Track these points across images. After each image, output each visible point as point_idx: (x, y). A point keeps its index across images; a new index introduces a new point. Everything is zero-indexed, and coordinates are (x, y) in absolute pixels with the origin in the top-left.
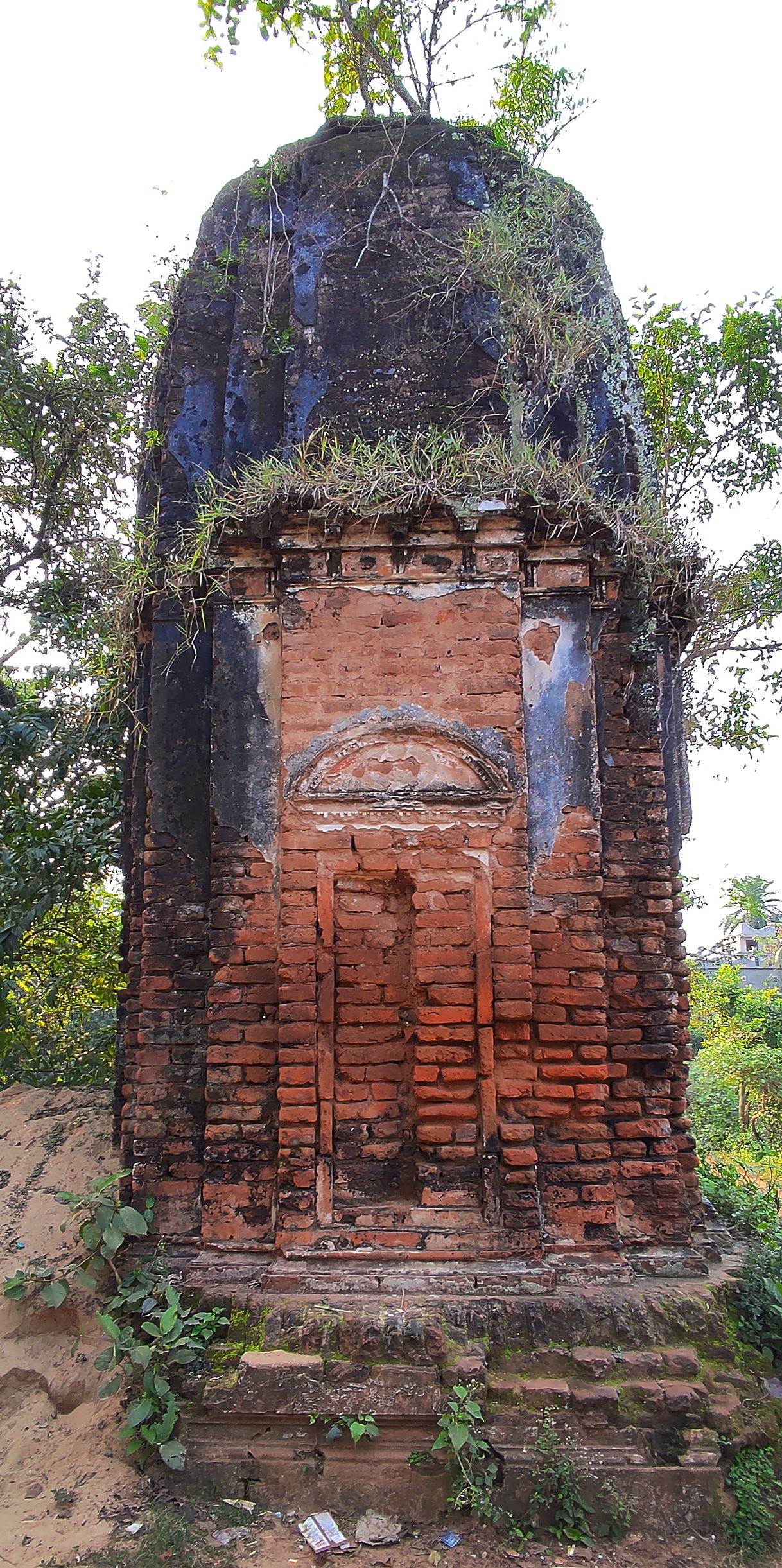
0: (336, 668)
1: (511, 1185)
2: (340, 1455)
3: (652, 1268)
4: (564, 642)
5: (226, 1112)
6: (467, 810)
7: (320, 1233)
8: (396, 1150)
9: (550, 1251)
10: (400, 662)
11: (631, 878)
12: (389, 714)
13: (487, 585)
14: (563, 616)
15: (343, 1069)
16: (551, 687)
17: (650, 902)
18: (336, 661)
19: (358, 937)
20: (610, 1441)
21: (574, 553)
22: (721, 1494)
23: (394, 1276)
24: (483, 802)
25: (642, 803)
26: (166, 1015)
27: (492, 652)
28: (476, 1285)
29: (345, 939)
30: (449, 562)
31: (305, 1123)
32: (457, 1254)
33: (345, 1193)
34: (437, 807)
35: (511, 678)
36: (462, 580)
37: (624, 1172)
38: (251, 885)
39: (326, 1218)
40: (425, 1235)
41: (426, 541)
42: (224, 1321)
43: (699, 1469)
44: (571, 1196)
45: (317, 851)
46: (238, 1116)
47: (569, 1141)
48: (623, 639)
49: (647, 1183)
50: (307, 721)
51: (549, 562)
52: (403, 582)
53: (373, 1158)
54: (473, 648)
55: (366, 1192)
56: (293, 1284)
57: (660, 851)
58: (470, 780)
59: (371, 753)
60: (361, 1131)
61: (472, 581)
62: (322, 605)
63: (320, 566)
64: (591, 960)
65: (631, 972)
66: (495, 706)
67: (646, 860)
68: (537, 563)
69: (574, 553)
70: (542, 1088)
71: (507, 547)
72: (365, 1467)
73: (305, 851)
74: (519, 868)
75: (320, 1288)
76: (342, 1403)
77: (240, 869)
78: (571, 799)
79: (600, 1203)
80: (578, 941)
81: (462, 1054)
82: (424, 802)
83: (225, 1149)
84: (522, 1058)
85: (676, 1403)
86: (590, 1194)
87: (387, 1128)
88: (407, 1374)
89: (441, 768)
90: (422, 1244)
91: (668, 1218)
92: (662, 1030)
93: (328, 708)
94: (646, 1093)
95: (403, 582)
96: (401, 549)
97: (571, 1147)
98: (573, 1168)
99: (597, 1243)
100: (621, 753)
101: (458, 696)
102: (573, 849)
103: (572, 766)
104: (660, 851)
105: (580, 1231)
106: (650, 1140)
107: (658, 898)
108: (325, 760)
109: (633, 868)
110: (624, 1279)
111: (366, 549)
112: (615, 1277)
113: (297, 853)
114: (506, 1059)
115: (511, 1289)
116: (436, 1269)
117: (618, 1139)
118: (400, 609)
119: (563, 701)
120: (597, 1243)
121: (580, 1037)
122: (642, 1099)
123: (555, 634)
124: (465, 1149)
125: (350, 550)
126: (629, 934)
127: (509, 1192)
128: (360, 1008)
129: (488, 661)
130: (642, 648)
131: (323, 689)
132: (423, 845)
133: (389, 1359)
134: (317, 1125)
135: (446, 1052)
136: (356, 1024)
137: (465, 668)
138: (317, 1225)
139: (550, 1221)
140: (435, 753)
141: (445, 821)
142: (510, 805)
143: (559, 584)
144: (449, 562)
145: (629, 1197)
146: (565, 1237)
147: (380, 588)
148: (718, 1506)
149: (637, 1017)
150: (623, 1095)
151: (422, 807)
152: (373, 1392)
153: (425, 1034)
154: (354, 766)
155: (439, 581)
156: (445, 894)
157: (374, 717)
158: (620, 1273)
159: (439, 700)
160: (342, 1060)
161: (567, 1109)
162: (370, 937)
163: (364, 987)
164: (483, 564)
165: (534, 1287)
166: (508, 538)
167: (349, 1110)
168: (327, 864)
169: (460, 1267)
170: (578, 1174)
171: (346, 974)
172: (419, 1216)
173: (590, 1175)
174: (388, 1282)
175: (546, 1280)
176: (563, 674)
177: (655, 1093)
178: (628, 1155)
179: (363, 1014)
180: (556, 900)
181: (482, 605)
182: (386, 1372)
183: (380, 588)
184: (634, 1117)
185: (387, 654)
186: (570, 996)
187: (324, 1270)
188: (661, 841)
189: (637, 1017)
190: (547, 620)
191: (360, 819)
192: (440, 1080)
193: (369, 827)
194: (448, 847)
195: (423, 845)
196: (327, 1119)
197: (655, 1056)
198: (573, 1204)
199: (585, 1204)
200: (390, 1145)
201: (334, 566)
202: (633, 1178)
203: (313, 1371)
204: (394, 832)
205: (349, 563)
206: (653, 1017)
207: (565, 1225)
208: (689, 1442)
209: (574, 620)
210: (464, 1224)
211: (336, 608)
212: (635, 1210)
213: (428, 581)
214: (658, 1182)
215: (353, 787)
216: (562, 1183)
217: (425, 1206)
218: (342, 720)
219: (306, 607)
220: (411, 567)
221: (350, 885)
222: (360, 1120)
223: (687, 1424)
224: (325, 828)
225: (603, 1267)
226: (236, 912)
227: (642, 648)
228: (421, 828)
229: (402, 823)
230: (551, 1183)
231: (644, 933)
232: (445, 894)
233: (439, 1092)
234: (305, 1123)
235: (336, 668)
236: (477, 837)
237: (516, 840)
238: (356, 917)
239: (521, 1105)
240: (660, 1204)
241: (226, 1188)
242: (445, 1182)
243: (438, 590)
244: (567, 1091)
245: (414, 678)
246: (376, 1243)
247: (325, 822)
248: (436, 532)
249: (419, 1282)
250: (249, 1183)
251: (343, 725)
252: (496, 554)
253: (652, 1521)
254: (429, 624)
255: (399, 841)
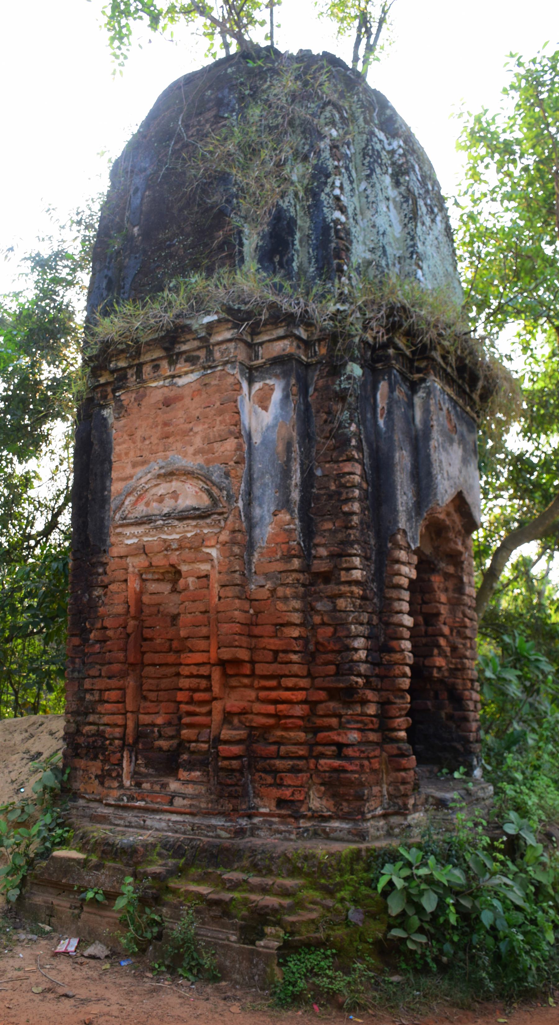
0: (138, 439)
1: (222, 769)
2: (90, 910)
3: (327, 834)
4: (277, 395)
5: (91, 718)
6: (201, 522)
7: (122, 792)
8: (175, 745)
9: (256, 815)
10: (171, 429)
11: (332, 556)
12: (163, 464)
13: (219, 368)
14: (277, 376)
15: (144, 693)
16: (268, 428)
17: (343, 573)
18: (139, 434)
19: (154, 609)
20: (224, 926)
21: (281, 332)
22: (276, 968)
23: (152, 821)
24: (209, 516)
25: (339, 500)
26: (77, 660)
27: (221, 412)
28: (193, 830)
29: (147, 611)
30: (198, 358)
31: (116, 725)
32: (188, 810)
33: (143, 770)
34: (185, 522)
35: (232, 428)
36: (205, 368)
37: (319, 767)
38: (106, 580)
39: (127, 783)
40: (173, 797)
41: (184, 348)
42: (66, 835)
43: (265, 950)
44: (270, 780)
45: (127, 556)
46: (97, 721)
47: (275, 743)
48: (330, 382)
49: (335, 775)
50: (124, 475)
51: (269, 341)
52: (173, 377)
53: (160, 749)
54: (211, 412)
55: (156, 770)
56: (103, 819)
57: (350, 534)
58: (205, 501)
59: (154, 491)
60: (153, 732)
61: (210, 367)
62: (133, 400)
63: (132, 376)
64: (287, 618)
65: (329, 625)
66: (222, 449)
67: (342, 543)
68: (261, 344)
69: (281, 332)
70: (258, 707)
71: (230, 340)
72: (99, 918)
73: (121, 557)
74: (232, 558)
75: (116, 822)
76: (89, 881)
77: (101, 570)
78: (278, 505)
79: (289, 786)
80: (280, 606)
81: (203, 683)
82: (178, 519)
83: (91, 740)
84: (245, 686)
85: (262, 908)
86: (281, 779)
87: (170, 731)
88: (119, 869)
89: (190, 495)
90: (171, 803)
91: (347, 800)
92: (347, 666)
93: (134, 465)
94: (343, 712)
95: (173, 377)
96: (172, 356)
97: (274, 748)
98: (272, 762)
99: (283, 812)
100: (327, 466)
101: (201, 445)
102: (279, 540)
103: (279, 481)
104: (350, 534)
105: (273, 803)
106: (340, 746)
107: (348, 569)
108: (129, 499)
109: (332, 549)
110: (293, 837)
111: (153, 361)
112: (287, 835)
113: (117, 559)
114: (235, 687)
115: (211, 834)
116: (175, 818)
117: (318, 744)
118: (172, 394)
119: (275, 436)
120: (283, 812)
121: (279, 672)
122: (340, 716)
123: (272, 390)
124: (203, 745)
125: (146, 363)
126: (328, 597)
127: (221, 774)
128: (157, 655)
129: (219, 419)
130: (342, 386)
131: (132, 454)
132: (180, 548)
133: (114, 860)
134: (125, 726)
135: (194, 682)
136: (154, 665)
137: (206, 426)
138: (121, 786)
139: (257, 795)
140: (187, 486)
141: (189, 530)
142: (226, 516)
143: (275, 354)
144: (198, 358)
145: (322, 784)
146: (265, 807)
147: (161, 383)
148: (273, 975)
149: (330, 657)
150: (321, 713)
151: (176, 523)
152: (103, 877)
153: (185, 671)
154: (145, 500)
155: (192, 372)
156: (198, 578)
157: (155, 468)
158: (290, 832)
159: (191, 450)
160: (145, 687)
161: (271, 721)
162: (161, 609)
163: (158, 641)
164: (217, 355)
165: (223, 834)
166: (228, 335)
167: (145, 719)
168: (136, 563)
169: (188, 818)
170: (274, 765)
171: (148, 633)
172: (174, 786)
173: (281, 767)
174: (149, 822)
175: (231, 830)
176: (276, 418)
177: (350, 712)
178: (322, 755)
179: (157, 658)
180: (267, 576)
181: (216, 382)
182: (110, 867)
183: (161, 383)
184: (330, 728)
185: (166, 424)
186: (274, 644)
187: (121, 812)
188: (352, 528)
189: (330, 657)
190: (268, 382)
191: (146, 534)
192: (191, 702)
193: (151, 539)
194: (196, 546)
195: (180, 548)
196: (131, 724)
197: (341, 685)
198: (271, 785)
199: (280, 785)
200: (172, 742)
201: (139, 373)
202: (325, 771)
203: (77, 861)
204: (165, 541)
205: (147, 369)
206: (342, 658)
207: (265, 799)
208: (266, 934)
209: (284, 378)
210: (197, 792)
211: (139, 400)
212: (324, 793)
213: (186, 373)
214: (342, 775)
215: (144, 514)
216: (265, 771)
217: (179, 780)
218: (140, 471)
219: (125, 403)
220: (178, 366)
221: (149, 576)
222: (154, 725)
223: (267, 923)
224: (129, 542)
225: (282, 828)
226: (99, 597)
227: (342, 386)
228: (177, 537)
229: (168, 534)
230: (258, 771)
231: (341, 596)
232: (198, 578)
233: (191, 708)
234: (116, 725)
235: (138, 439)
236: (209, 539)
237: (231, 539)
238: (154, 596)
239: (243, 718)
240: (342, 790)
241: (90, 763)
242: (190, 766)
243: (192, 377)
244: (271, 709)
245: (178, 438)
246: (148, 799)
247: (128, 538)
248: (189, 340)
249: (164, 824)
250: (102, 761)
251: (139, 475)
252: (224, 346)
253: (236, 976)
254: (187, 401)
255: (167, 547)
